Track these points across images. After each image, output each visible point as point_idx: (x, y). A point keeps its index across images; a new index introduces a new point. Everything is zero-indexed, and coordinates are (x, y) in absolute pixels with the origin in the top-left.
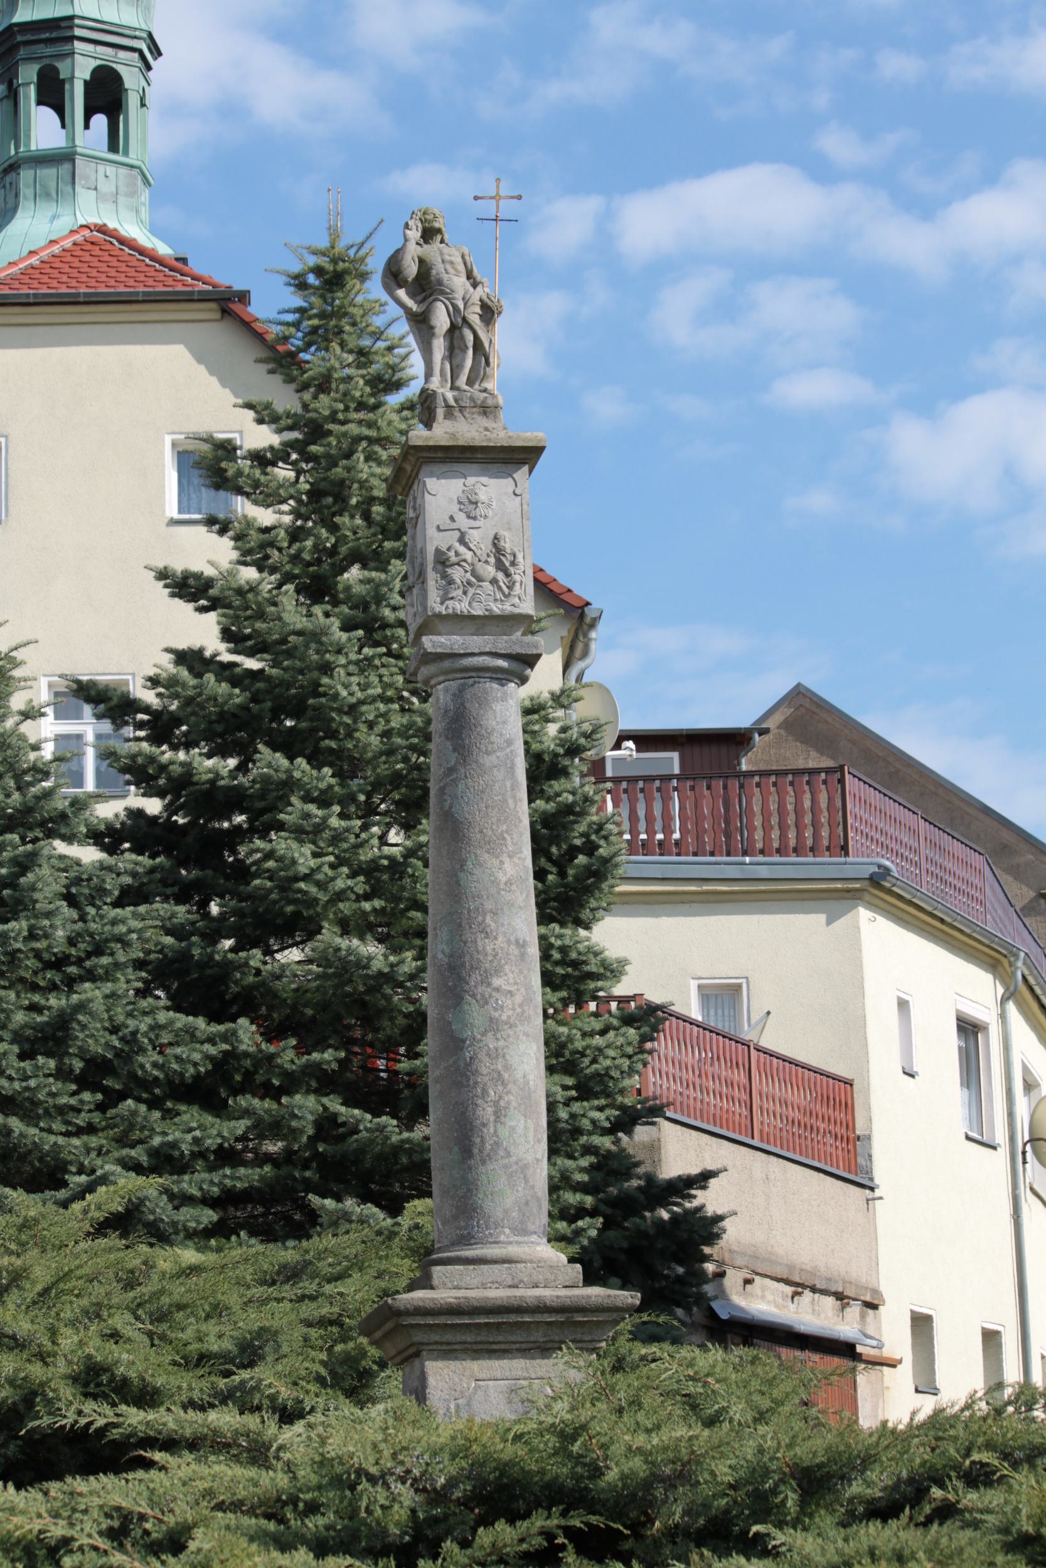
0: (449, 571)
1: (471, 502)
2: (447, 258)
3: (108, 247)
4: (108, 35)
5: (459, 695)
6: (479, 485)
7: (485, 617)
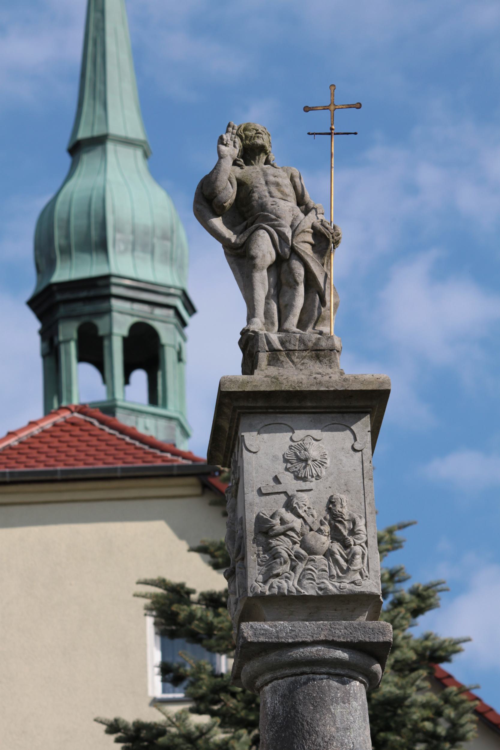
0: (274, 542)
1: (300, 460)
2: (271, 179)
3: (89, 427)
4: (145, 293)
5: (289, 698)
6: (309, 440)
7: (318, 598)
